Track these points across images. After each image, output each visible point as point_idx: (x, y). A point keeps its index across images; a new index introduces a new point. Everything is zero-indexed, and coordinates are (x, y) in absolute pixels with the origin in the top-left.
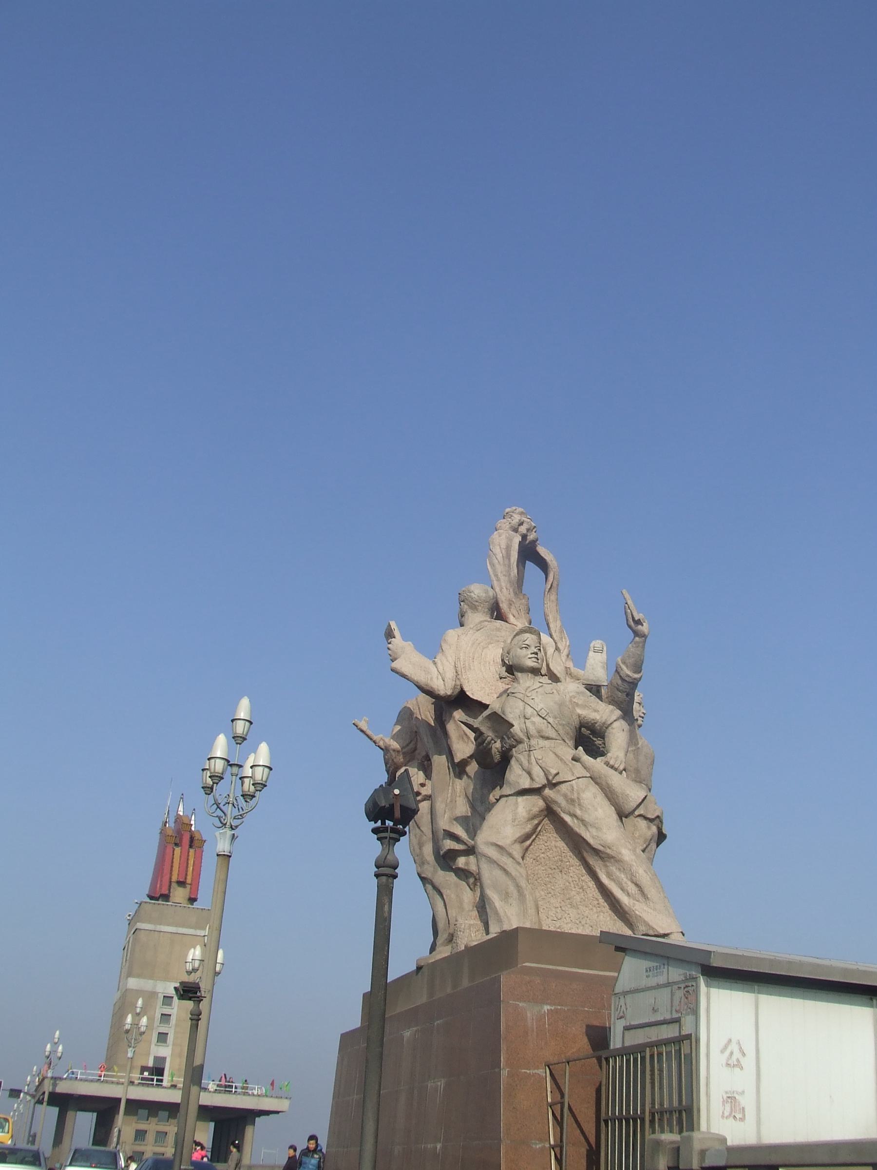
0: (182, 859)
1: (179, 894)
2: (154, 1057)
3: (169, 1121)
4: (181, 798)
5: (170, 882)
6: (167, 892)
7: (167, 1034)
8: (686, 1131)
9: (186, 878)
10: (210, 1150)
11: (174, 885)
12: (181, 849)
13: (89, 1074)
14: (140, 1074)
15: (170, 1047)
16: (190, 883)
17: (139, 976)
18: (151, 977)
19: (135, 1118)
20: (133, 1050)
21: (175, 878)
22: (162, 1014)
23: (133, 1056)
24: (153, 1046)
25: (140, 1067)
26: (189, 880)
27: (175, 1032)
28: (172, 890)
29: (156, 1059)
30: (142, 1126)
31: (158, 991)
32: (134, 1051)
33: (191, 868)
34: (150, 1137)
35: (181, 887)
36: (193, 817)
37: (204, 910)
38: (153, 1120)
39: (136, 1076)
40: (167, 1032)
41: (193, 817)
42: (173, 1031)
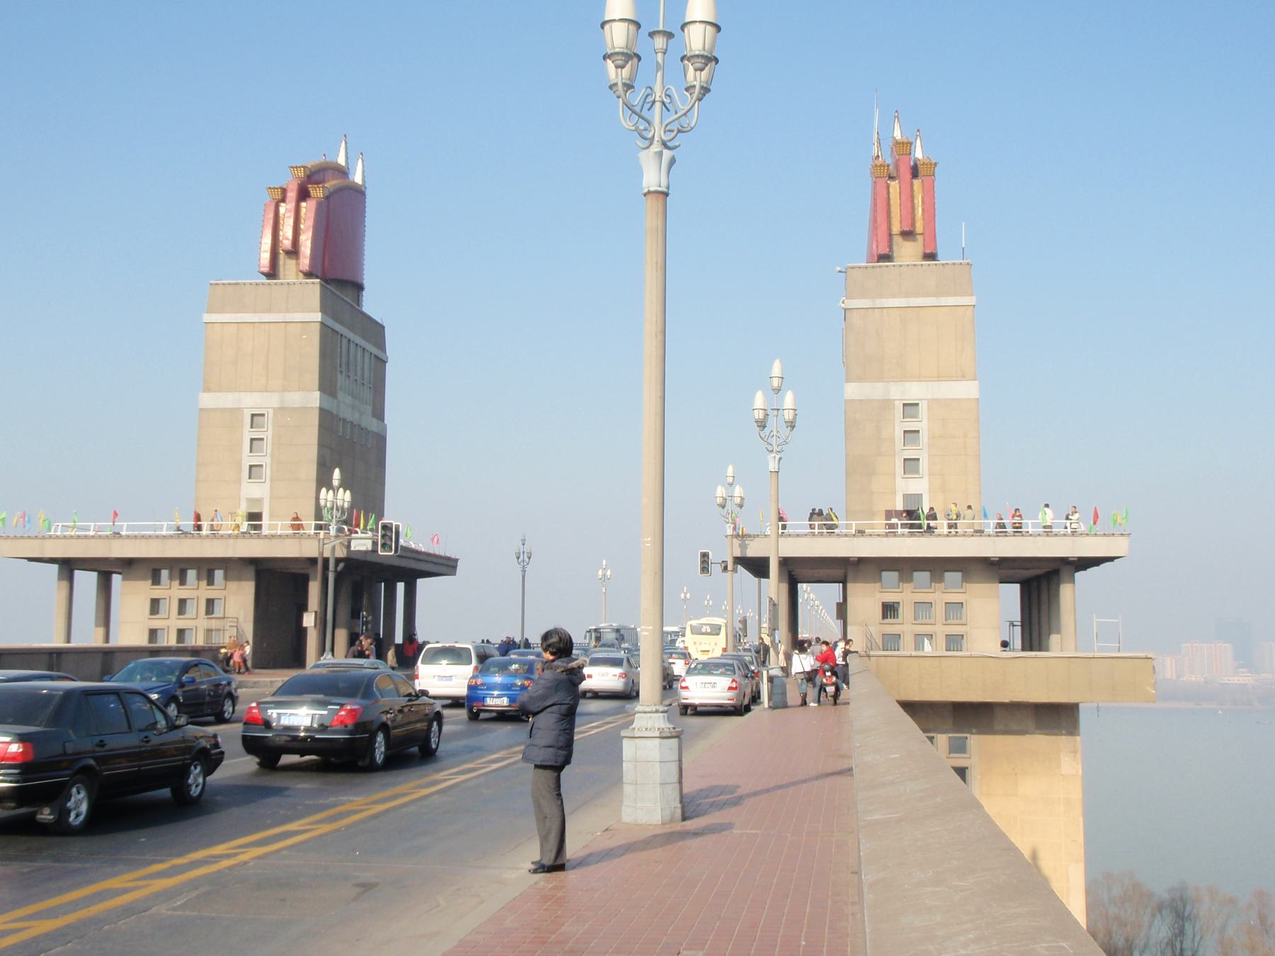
0: (903, 197)
1: (907, 252)
2: (904, 495)
3: (901, 587)
4: (895, 117)
5: (890, 235)
6: (888, 250)
7: (918, 459)
9: (913, 224)
10: (1019, 624)
11: (898, 240)
12: (899, 182)
14: (886, 520)
15: (926, 479)
17: (860, 379)
18: (880, 378)
19: (878, 585)
20: (778, 457)
21: (896, 229)
22: (905, 432)
24: (899, 480)
26: (919, 228)
27: (929, 455)
28: (895, 248)
29: (906, 497)
30: (890, 598)
31: (894, 398)
32: (780, 459)
33: (920, 209)
34: (906, 612)
35: (908, 241)
36: (918, 140)
37: (946, 266)
38: (907, 587)
40: (918, 457)
41: (918, 140)
42: (926, 455)
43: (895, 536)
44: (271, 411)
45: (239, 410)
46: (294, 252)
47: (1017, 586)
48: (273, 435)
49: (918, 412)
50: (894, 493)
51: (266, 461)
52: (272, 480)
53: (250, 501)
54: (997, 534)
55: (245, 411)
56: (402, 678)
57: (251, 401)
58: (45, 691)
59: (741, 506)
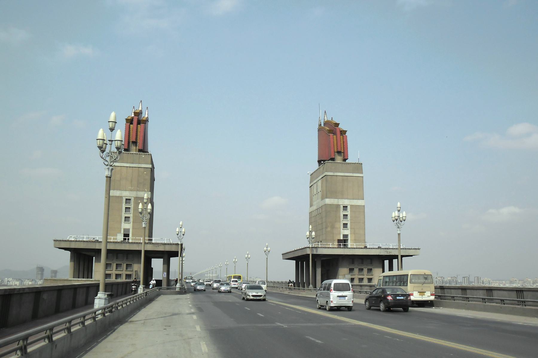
7: (347, 224)
8: (233, 278)
13: (324, 245)
15: (349, 230)
16: (343, 152)
23: (147, 202)
24: (341, 230)
25: (337, 240)
27: (350, 223)
39: (336, 243)
43: (340, 248)
44: (133, 198)
45: (121, 197)
46: (135, 143)
47: (171, 259)
48: (134, 206)
49: (347, 209)
50: (340, 234)
51: (131, 216)
52: (133, 222)
53: (125, 230)
54: (338, 248)
55: (124, 198)
56: (103, 294)
57: (126, 194)
58: (306, 314)
59: (183, 235)
